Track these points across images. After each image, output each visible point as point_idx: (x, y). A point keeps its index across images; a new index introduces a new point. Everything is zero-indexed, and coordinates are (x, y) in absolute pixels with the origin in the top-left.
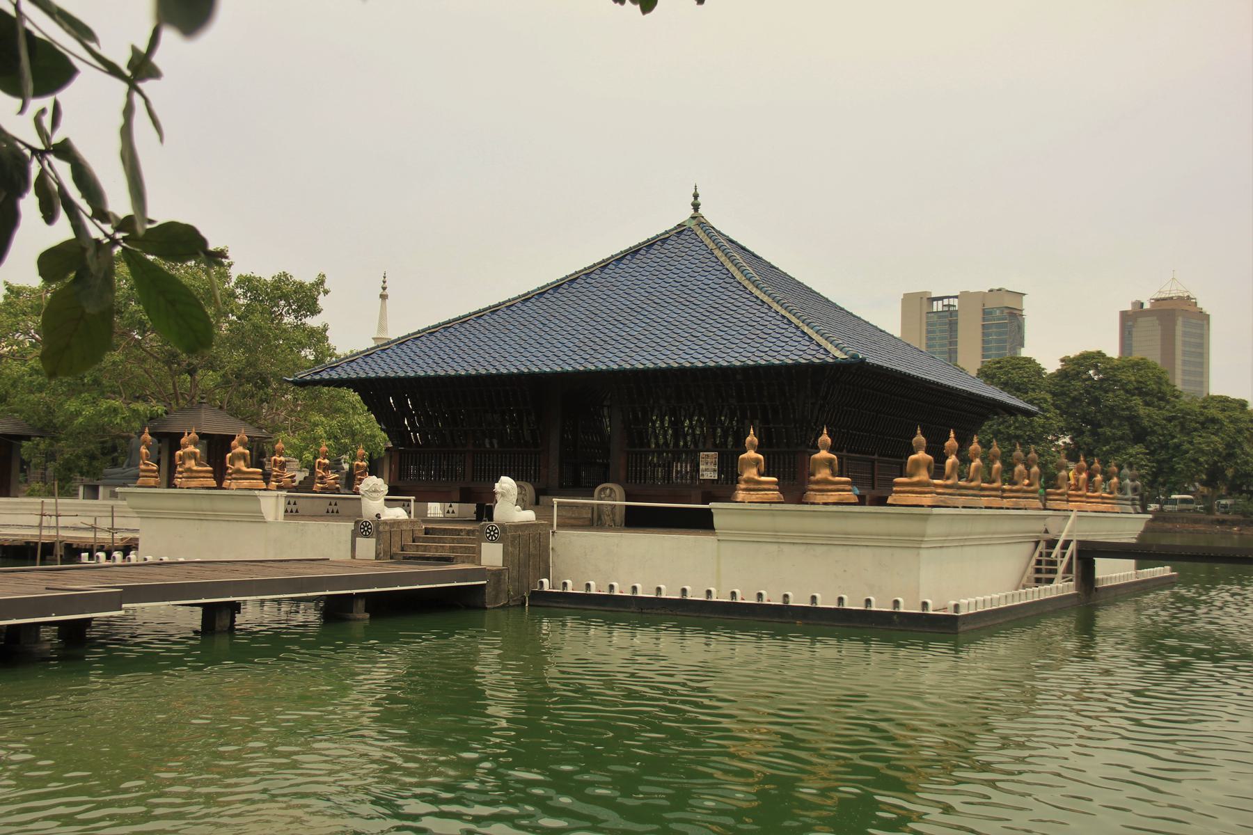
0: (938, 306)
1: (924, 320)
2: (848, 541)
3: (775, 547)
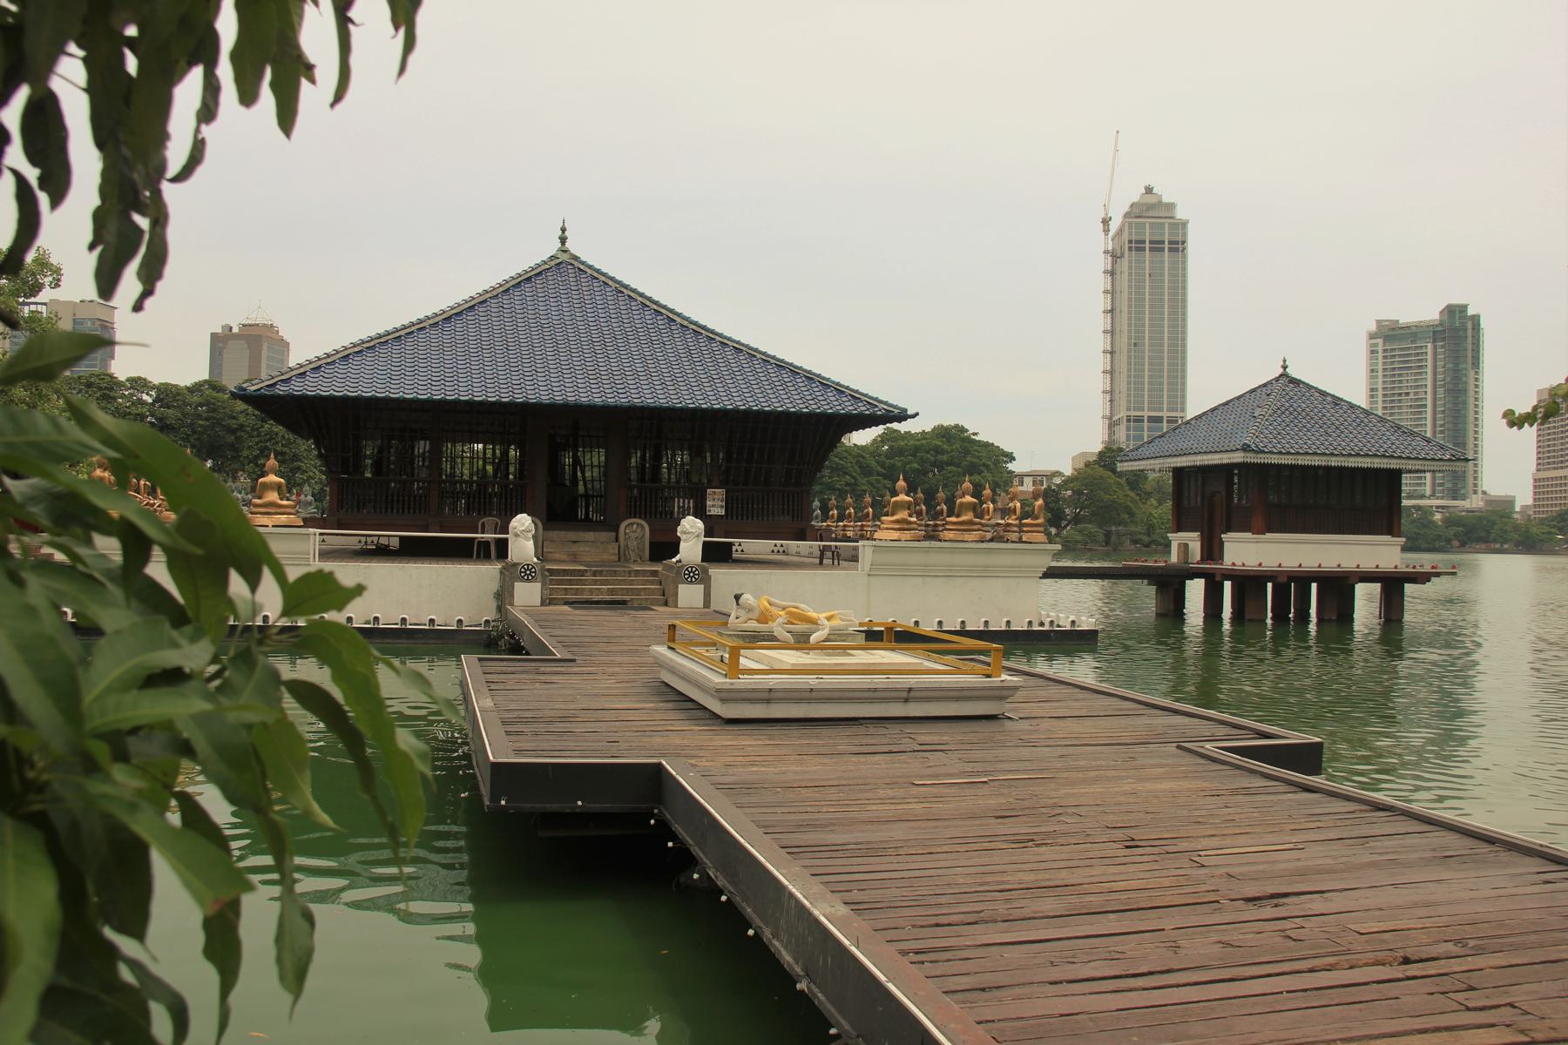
2: (985, 573)
3: (920, 580)
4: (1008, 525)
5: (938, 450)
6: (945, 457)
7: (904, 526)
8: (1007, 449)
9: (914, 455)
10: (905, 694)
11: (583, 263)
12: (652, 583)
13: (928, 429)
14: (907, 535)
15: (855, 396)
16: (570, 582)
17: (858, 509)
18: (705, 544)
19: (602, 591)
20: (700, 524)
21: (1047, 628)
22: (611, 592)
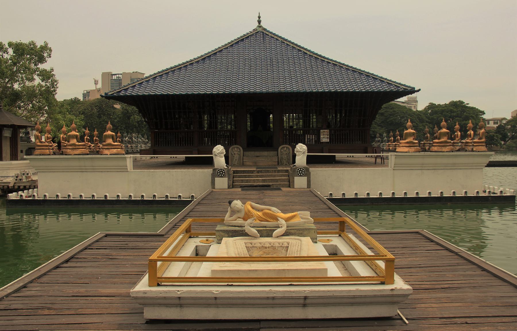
0: (114, 77)
1: (110, 82)
2: (454, 167)
4: (467, 143)
5: (452, 111)
6: (455, 114)
7: (411, 145)
8: (481, 110)
9: (442, 114)
10: (302, 301)
11: (268, 31)
12: (284, 176)
13: (447, 103)
14: (413, 149)
15: (389, 83)
16: (245, 177)
17: (395, 137)
18: (308, 157)
19: (259, 180)
20: (305, 147)
21: (487, 194)
22: (264, 181)
